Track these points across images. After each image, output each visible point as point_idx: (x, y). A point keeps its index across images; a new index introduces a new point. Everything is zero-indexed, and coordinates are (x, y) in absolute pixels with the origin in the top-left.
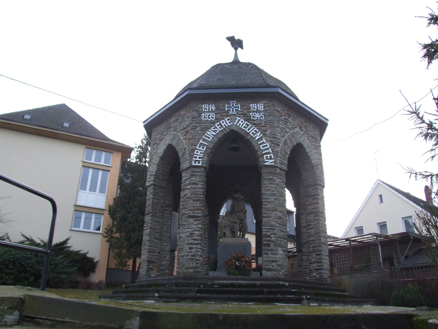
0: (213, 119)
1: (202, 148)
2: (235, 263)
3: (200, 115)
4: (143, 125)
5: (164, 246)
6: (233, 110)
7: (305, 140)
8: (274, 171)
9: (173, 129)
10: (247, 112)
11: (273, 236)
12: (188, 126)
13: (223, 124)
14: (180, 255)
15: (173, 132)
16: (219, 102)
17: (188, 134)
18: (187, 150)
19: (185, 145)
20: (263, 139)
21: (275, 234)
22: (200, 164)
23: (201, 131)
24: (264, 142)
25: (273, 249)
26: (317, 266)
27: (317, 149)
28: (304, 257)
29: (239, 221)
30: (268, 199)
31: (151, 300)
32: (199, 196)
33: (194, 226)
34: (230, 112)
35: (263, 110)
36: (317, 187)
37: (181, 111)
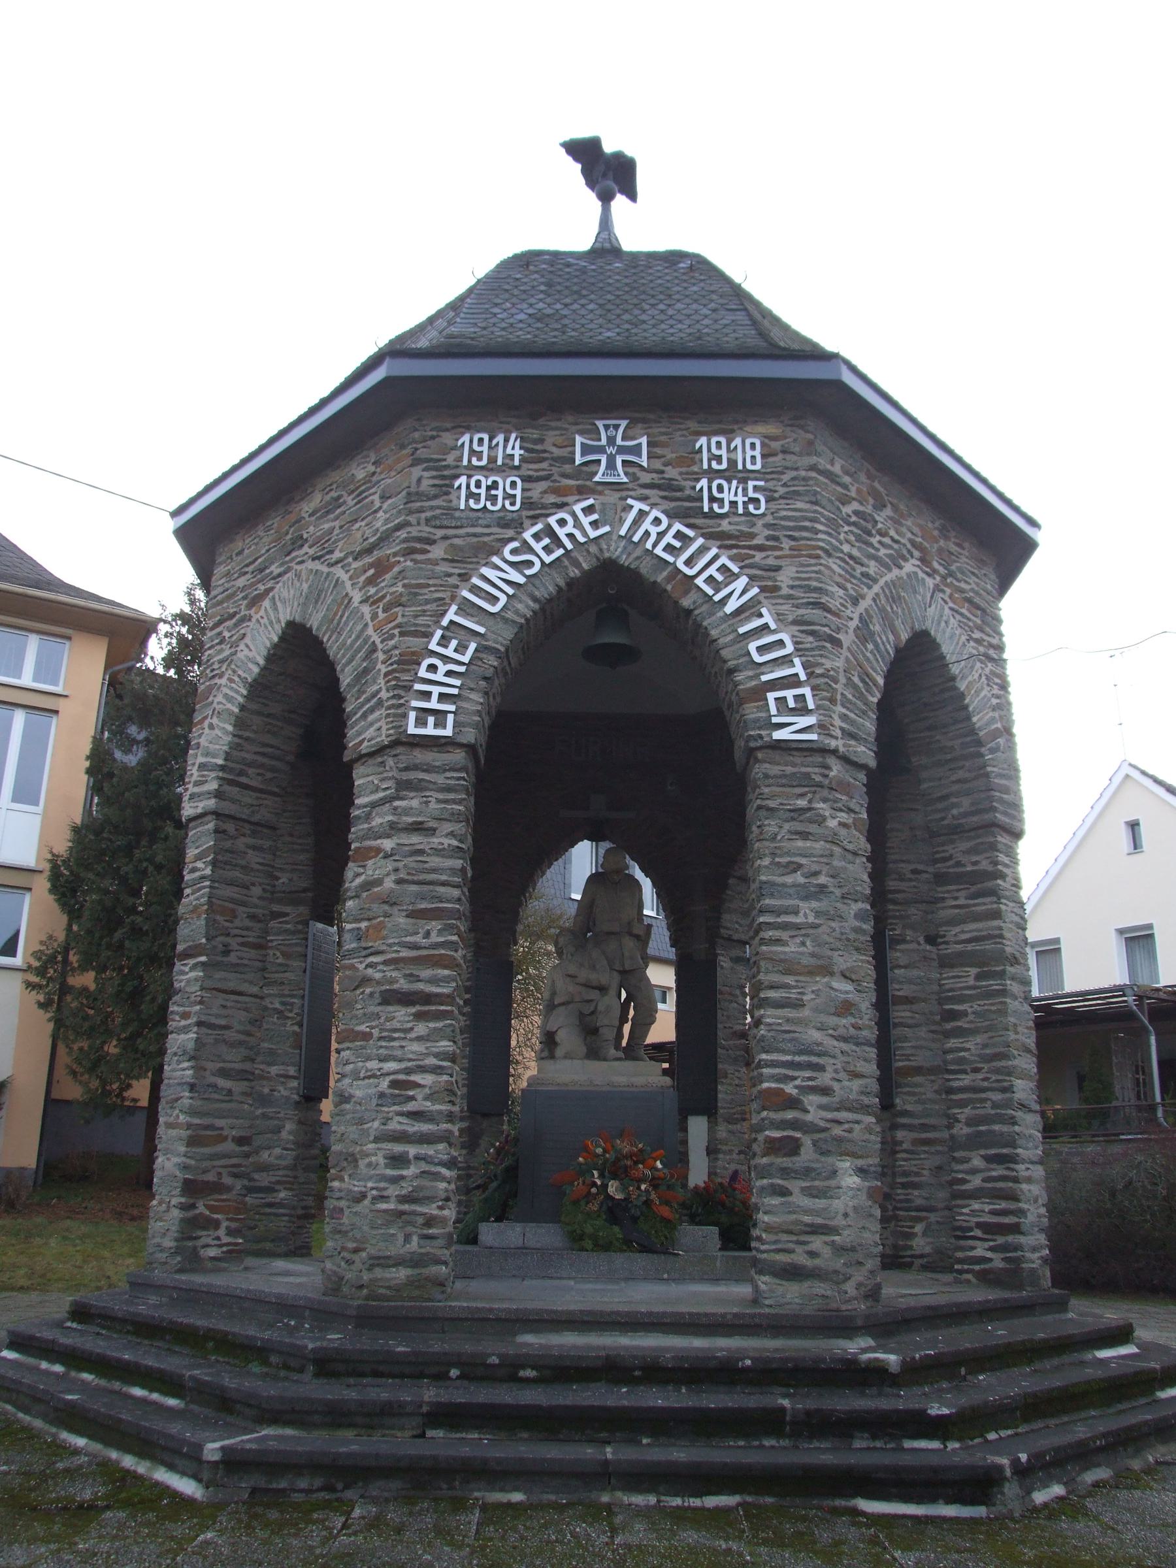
0: (513, 504)
1: (456, 650)
2: (605, 1186)
3: (447, 482)
4: (171, 525)
5: (269, 1079)
6: (611, 465)
7: (945, 618)
8: (817, 770)
9: (311, 551)
10: (681, 474)
11: (812, 1101)
12: (385, 538)
13: (561, 532)
14: (340, 1190)
15: (311, 565)
16: (541, 421)
17: (388, 576)
18: (381, 656)
19: (370, 631)
20: (764, 611)
21: (825, 1091)
22: (445, 727)
23: (452, 561)
24: (765, 628)
25: (814, 1169)
26: (994, 1213)
27: (991, 659)
28: (900, 1134)
29: (615, 974)
30: (786, 913)
31: (183, 1473)
32: (442, 889)
33: (416, 1047)
34: (596, 473)
35: (758, 467)
36: (992, 840)
37: (354, 465)
